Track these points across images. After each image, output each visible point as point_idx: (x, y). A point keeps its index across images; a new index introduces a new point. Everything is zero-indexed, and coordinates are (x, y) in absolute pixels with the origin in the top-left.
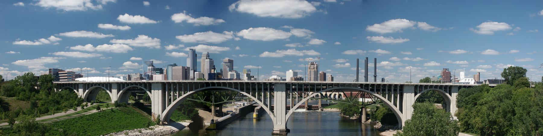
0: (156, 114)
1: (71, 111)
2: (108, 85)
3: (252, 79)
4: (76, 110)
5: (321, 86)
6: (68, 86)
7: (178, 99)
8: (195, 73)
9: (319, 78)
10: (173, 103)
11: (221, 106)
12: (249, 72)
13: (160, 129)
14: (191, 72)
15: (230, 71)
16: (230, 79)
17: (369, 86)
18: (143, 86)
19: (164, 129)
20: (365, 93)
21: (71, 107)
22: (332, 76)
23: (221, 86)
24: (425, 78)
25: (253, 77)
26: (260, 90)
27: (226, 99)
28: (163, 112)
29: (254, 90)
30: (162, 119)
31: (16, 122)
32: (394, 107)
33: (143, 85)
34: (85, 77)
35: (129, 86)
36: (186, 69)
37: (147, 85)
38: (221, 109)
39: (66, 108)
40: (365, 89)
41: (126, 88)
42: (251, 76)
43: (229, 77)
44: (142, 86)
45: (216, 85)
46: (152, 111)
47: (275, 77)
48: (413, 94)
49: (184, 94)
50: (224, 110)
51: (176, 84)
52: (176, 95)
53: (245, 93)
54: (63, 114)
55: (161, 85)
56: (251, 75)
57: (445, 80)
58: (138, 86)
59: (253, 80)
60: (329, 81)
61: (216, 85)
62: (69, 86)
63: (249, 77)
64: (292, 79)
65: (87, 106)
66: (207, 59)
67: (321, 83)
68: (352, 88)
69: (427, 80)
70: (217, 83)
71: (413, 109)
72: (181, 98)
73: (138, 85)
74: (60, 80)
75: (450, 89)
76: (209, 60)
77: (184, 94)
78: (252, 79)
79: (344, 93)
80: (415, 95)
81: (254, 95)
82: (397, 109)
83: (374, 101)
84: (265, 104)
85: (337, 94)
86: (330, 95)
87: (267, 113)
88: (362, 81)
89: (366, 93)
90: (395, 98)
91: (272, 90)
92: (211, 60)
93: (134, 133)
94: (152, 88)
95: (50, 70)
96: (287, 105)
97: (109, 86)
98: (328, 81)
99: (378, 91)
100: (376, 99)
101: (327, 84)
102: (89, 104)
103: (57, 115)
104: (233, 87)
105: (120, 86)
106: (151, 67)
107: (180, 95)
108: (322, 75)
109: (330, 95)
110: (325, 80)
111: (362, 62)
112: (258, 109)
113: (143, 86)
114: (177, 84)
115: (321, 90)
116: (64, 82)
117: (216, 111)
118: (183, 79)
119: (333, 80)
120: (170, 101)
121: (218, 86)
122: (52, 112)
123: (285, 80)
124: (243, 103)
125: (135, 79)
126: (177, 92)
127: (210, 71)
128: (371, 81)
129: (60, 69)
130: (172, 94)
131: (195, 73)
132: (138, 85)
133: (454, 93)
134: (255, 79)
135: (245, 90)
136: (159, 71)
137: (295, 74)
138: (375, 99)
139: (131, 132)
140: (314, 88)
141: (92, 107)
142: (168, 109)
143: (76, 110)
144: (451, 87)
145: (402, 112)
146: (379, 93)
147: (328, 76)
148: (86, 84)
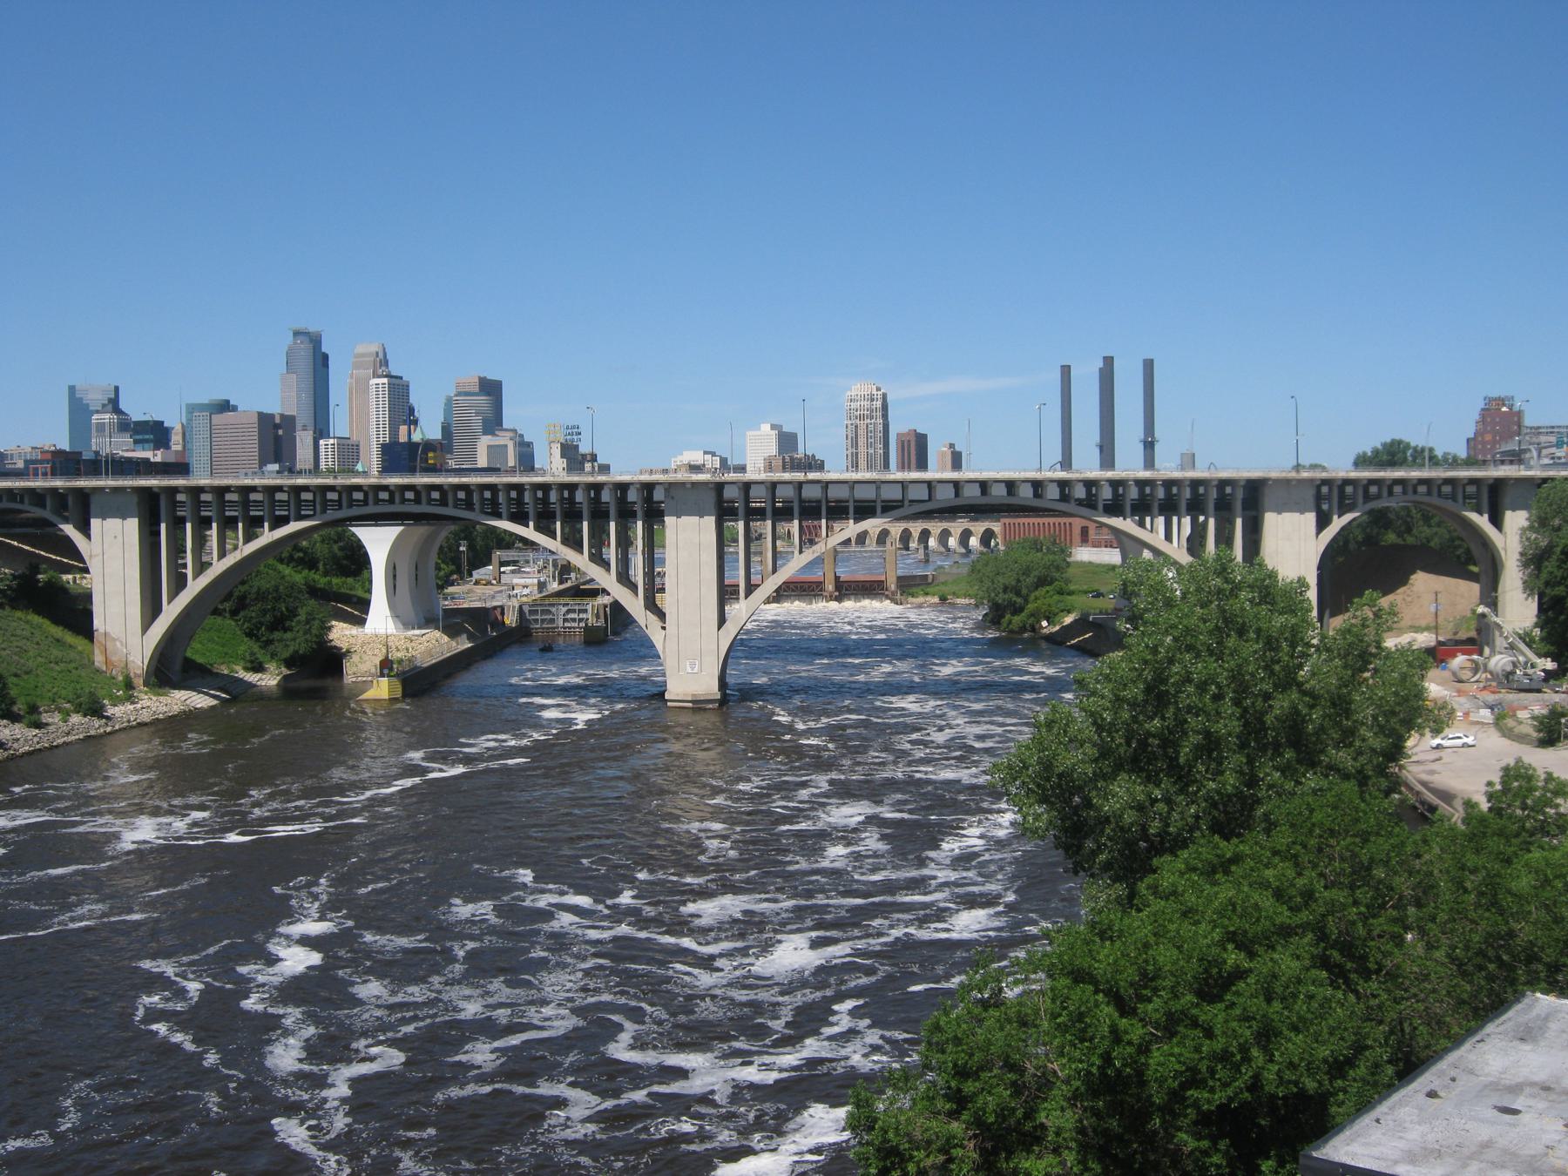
7: (219, 567)
8: (322, 442)
9: (862, 463)
10: (195, 587)
14: (304, 440)
15: (485, 433)
22: (957, 449)
24: (1380, 447)
28: (146, 627)
29: (572, 516)
30: (146, 662)
36: (277, 427)
42: (584, 456)
43: (482, 462)
46: (98, 623)
47: (697, 457)
48: (1310, 518)
53: (529, 532)
55: (135, 499)
56: (584, 448)
57: (1485, 455)
58: (26, 507)
60: (943, 469)
64: (769, 467)
66: (376, 375)
69: (1393, 454)
75: (1495, 498)
76: (385, 380)
78: (588, 466)
80: (1322, 523)
81: (573, 542)
84: (625, 579)
85: (979, 528)
87: (635, 621)
88: (1087, 466)
90: (625, 543)
91: (654, 515)
92: (397, 381)
94: (93, 508)
98: (937, 471)
99: (1114, 509)
106: (107, 416)
110: (922, 464)
112: (605, 606)
115: (879, 510)
120: (179, 583)
123: (742, 469)
124: (536, 581)
127: (394, 431)
128: (1129, 466)
131: (322, 442)
133: (1514, 510)
134: (605, 469)
136: (147, 437)
137: (787, 441)
142: (171, 611)
144: (1497, 486)
145: (88, 536)
147: (936, 450)
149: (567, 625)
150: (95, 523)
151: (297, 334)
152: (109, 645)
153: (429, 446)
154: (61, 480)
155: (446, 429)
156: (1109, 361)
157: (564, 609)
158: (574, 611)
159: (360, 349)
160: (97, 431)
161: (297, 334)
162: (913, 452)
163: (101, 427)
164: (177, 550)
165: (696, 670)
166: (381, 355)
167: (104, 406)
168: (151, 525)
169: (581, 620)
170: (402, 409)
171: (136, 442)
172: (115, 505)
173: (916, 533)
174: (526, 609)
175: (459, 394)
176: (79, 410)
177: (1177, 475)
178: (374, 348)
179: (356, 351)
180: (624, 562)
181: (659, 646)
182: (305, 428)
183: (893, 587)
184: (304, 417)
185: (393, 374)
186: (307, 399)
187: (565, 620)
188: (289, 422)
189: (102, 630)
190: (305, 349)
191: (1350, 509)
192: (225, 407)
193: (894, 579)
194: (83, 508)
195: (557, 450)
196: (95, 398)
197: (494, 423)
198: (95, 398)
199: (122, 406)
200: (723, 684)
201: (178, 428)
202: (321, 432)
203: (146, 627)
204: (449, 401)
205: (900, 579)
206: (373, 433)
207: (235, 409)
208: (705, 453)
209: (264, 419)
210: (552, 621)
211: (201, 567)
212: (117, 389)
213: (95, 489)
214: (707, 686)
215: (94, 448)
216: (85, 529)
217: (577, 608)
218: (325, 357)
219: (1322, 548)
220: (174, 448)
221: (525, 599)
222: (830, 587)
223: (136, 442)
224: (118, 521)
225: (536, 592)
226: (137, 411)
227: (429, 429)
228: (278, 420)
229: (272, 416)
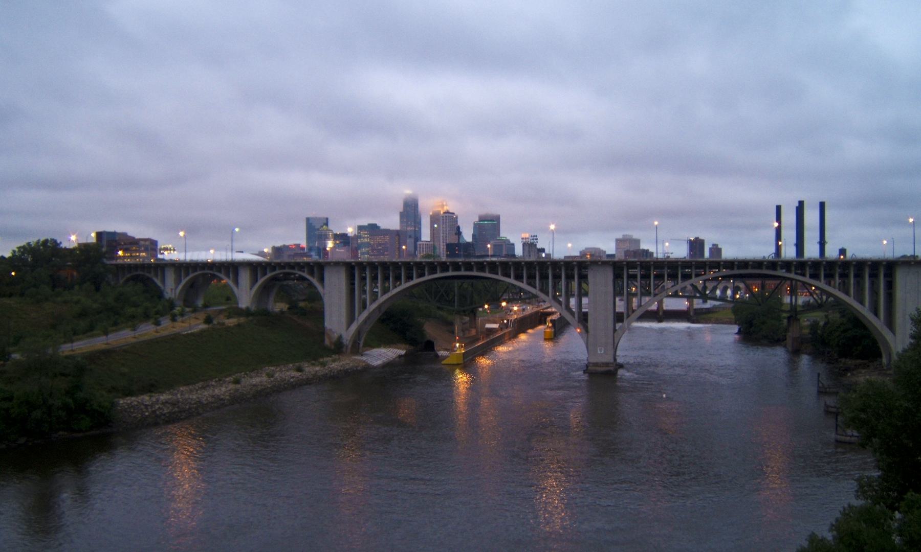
1: (147, 331)
5: (691, 269)
7: (382, 299)
12: (535, 241)
16: (492, 256)
20: (796, 284)
21: (146, 317)
27: (435, 298)
28: (350, 323)
31: (13, 356)
32: (870, 316)
39: (133, 321)
40: (796, 274)
41: (270, 275)
44: (304, 271)
49: (393, 288)
51: (424, 266)
52: (376, 290)
68: (765, 271)
71: (683, 257)
77: (395, 287)
79: (745, 284)
82: (878, 323)
83: (819, 301)
89: (798, 283)
90: (874, 293)
100: (824, 297)
104: (499, 274)
107: (385, 291)
111: (789, 218)
118: (352, 258)
126: (379, 285)
130: (368, 288)
135: (525, 280)
138: (822, 297)
139: (281, 371)
140: (677, 274)
145: (894, 333)
146: (832, 283)
216: (322, 280)
219: (252, 296)
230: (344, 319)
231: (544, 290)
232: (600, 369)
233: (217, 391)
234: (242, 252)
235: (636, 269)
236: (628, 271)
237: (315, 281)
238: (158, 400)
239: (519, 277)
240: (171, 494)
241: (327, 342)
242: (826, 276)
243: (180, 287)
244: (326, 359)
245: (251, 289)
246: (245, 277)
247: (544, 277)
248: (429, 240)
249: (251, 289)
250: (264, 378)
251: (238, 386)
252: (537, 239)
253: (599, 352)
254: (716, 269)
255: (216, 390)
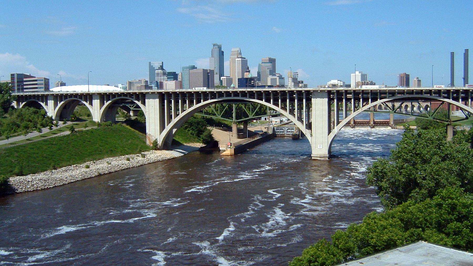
0: (152, 136)
1: (34, 134)
2: (88, 97)
3: (300, 85)
4: (41, 132)
6: (33, 99)
7: (182, 115)
11: (246, 123)
13: (157, 156)
14: (216, 78)
16: (269, 87)
17: (460, 93)
18: (134, 98)
19: (162, 156)
22: (419, 79)
23: (231, 96)
25: (302, 82)
26: (357, 99)
27: (220, 115)
28: (161, 132)
33: (134, 97)
34: (67, 86)
35: (115, 97)
36: (208, 73)
37: (140, 96)
38: (246, 127)
42: (299, 82)
43: (269, 84)
44: (133, 98)
45: (232, 95)
47: (335, 82)
50: (251, 128)
54: (22, 138)
55: (158, 95)
58: (128, 98)
59: (301, 87)
61: (232, 95)
62: (35, 99)
63: (296, 82)
65: (57, 126)
67: (404, 90)
70: (249, 92)
72: (185, 113)
73: (128, 96)
74: (25, 90)
76: (240, 59)
77: (189, 107)
84: (300, 119)
86: (400, 107)
90: (300, 108)
93: (120, 162)
95: (13, 75)
96: (375, 121)
97: (89, 97)
101: (413, 90)
102: (61, 123)
103: (11, 140)
105: (103, 97)
106: (160, 71)
108: (403, 79)
109: (400, 107)
113: (134, 98)
114: (202, 95)
116: (30, 94)
117: (239, 131)
119: (409, 85)
120: (170, 117)
121: (242, 96)
122: (56, 139)
123: (349, 86)
124: (279, 120)
125: (137, 87)
127: (243, 74)
129: (28, 74)
132: (127, 97)
134: (306, 86)
136: (171, 77)
139: (116, 160)
141: (65, 127)
143: (40, 131)
148: (58, 96)
149: (288, 133)
150: (147, 101)
151: (214, 45)
152: (151, 137)
153: (251, 79)
154: (249, 89)
155: (259, 74)
156: (467, 51)
157: (287, 129)
158: (290, 129)
159: (233, 50)
160: (157, 75)
161: (214, 45)
162: (405, 80)
163: (158, 74)
164: (169, 109)
165: (321, 148)
166: (239, 51)
167: (159, 68)
168: (162, 101)
169: (292, 132)
170: (246, 68)
171: (168, 78)
172: (153, 95)
173: (403, 105)
174: (275, 128)
175: (262, 63)
176: (152, 69)
177: (293, 89)
178: (237, 49)
179: (232, 50)
180: (301, 114)
181: (310, 140)
182: (217, 74)
183: (392, 123)
184: (217, 71)
185: (243, 57)
186: (217, 66)
187: (287, 132)
188: (212, 72)
189: (148, 133)
190: (217, 51)
191: (62, 101)
192: (194, 67)
193: (393, 121)
194: (142, 97)
195: (290, 80)
196: (157, 65)
197: (273, 72)
198: (157, 65)
199: (164, 68)
200: (330, 152)
201: (180, 74)
202: (221, 74)
203: (161, 132)
204: (260, 65)
205: (394, 121)
206: (237, 76)
207: (196, 68)
208: (338, 81)
209: (205, 71)
210: (283, 132)
211: (177, 115)
212: (162, 63)
213: (147, 93)
214: (325, 152)
215: (156, 80)
216: (144, 103)
217: (291, 128)
218: (223, 52)
219: (101, 113)
220: (179, 80)
221: (275, 125)
222: (372, 123)
223: (168, 78)
224: (96, 100)
225: (279, 123)
226: (168, 69)
227: (253, 73)
228: (209, 72)
229: (207, 70)
230: (158, 128)
231: (284, 108)
232: (322, 159)
233: (74, 173)
234: (108, 85)
235: (386, 94)
236: (452, 95)
237: (139, 103)
238: (35, 178)
239: (268, 101)
240: (339, 248)
241: (148, 142)
242: (274, 101)
243: (57, 108)
244: (146, 153)
245: (100, 109)
246: (96, 102)
247: (284, 101)
248: (257, 76)
249: (100, 109)
250: (106, 165)
251: (88, 170)
252: (298, 75)
253: (319, 148)
254: (428, 94)
255: (73, 172)
